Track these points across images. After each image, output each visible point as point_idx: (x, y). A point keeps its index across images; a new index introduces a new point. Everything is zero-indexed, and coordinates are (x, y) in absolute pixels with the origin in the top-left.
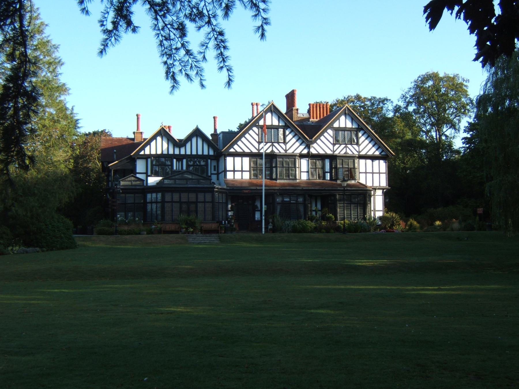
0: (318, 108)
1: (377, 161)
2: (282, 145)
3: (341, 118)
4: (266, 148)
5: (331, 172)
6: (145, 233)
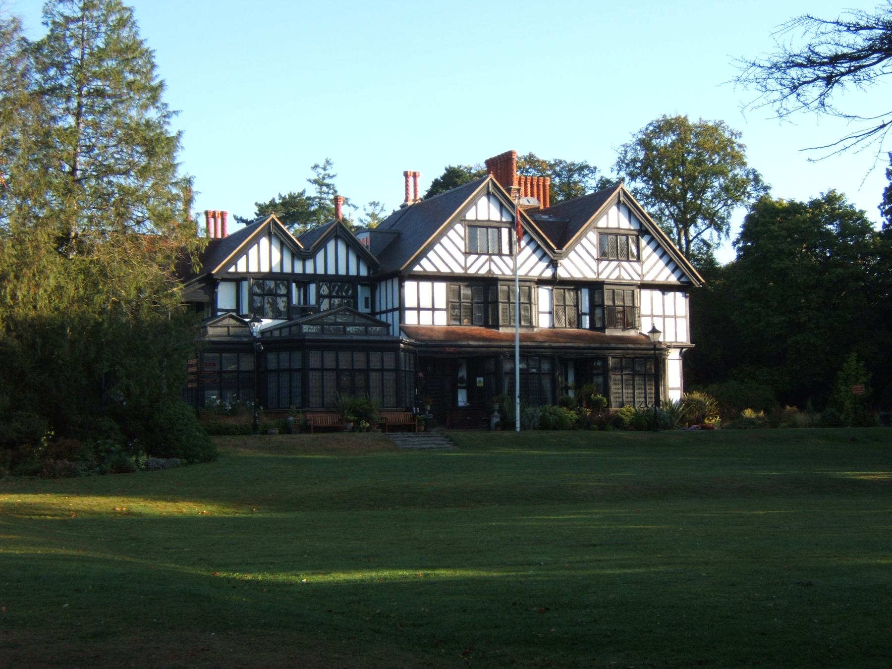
0: (529, 186)
1: (672, 294)
2: (507, 259)
3: (610, 212)
4: (478, 266)
5: (592, 314)
6: (277, 430)
